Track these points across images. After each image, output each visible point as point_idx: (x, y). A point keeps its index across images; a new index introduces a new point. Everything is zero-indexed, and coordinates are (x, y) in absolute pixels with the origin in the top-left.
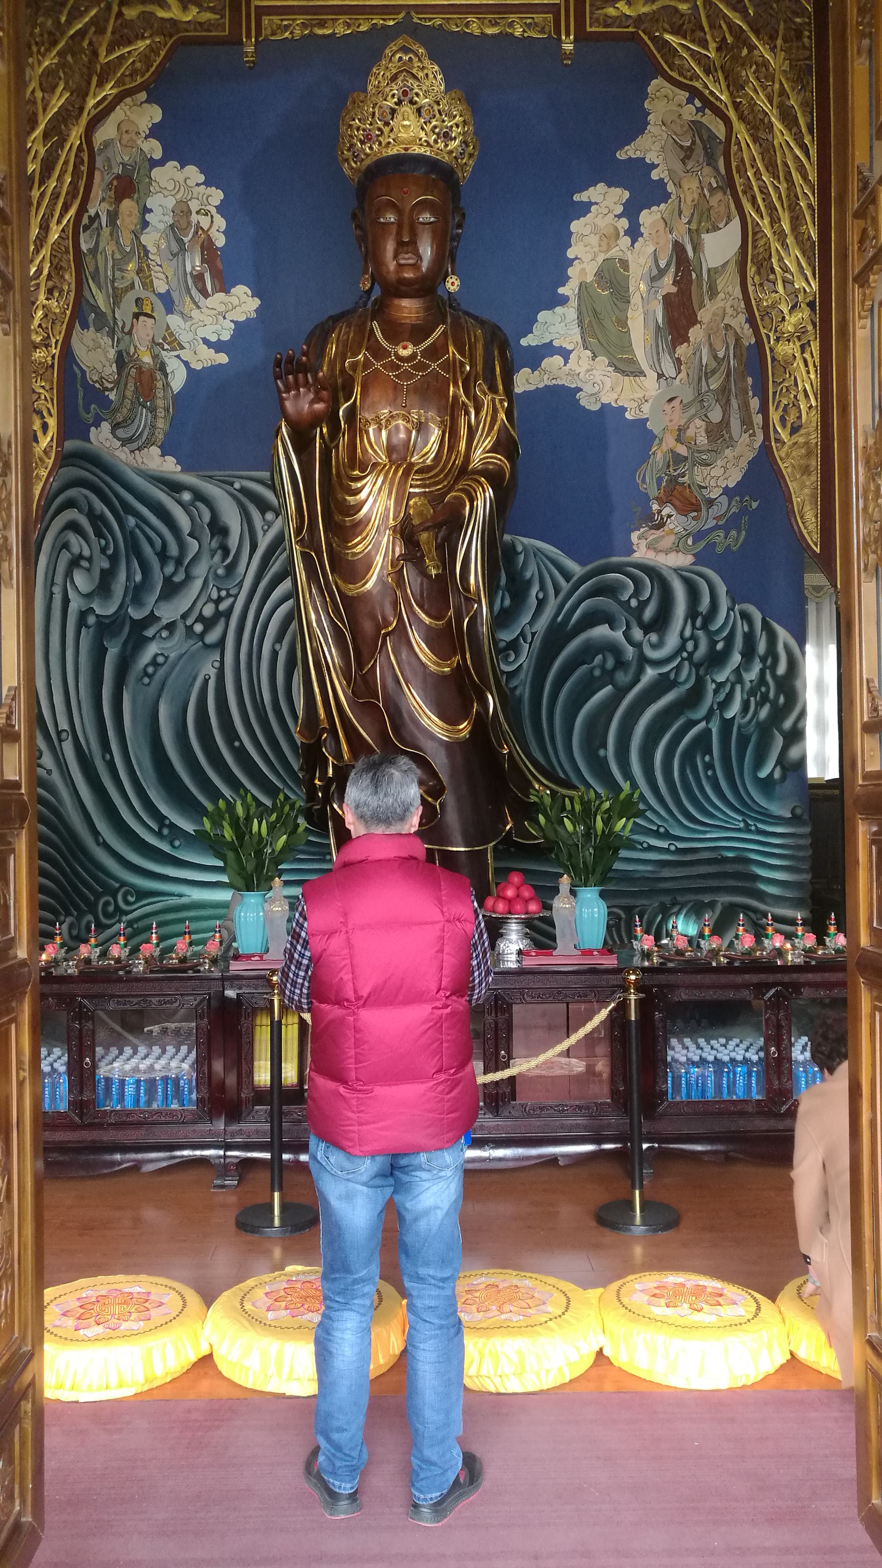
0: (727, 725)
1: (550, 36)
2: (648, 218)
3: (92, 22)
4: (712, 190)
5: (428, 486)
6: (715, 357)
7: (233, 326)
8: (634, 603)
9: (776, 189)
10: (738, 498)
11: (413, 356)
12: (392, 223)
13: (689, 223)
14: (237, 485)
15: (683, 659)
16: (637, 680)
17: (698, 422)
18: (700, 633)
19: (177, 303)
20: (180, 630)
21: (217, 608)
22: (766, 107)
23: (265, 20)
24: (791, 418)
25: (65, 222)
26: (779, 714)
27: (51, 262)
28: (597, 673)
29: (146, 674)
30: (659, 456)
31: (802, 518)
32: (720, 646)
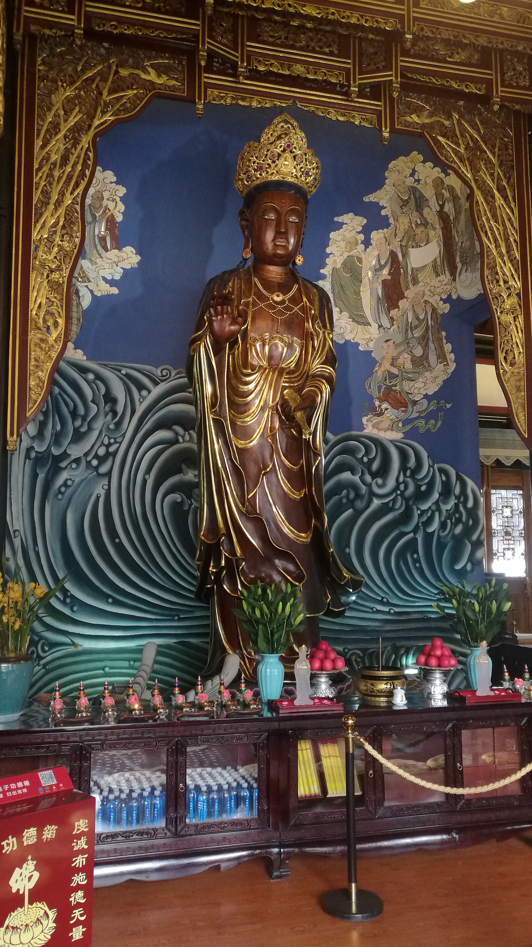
0: (428, 537)
1: (375, 127)
2: (375, 236)
3: (98, 73)
4: (417, 225)
5: (293, 382)
6: (418, 318)
7: (122, 271)
8: (365, 459)
9: (498, 229)
10: (435, 401)
11: (283, 302)
12: (273, 220)
13: (401, 241)
14: (123, 372)
15: (397, 495)
16: (368, 506)
17: (406, 355)
18: (409, 480)
19: (88, 253)
20: (83, 464)
21: (107, 449)
22: (491, 184)
23: (209, 91)
24: (510, 358)
25: (76, 194)
26: (468, 531)
27: (65, 217)
28: (344, 501)
29: (60, 492)
30: (380, 373)
31: (517, 416)
32: (423, 488)
